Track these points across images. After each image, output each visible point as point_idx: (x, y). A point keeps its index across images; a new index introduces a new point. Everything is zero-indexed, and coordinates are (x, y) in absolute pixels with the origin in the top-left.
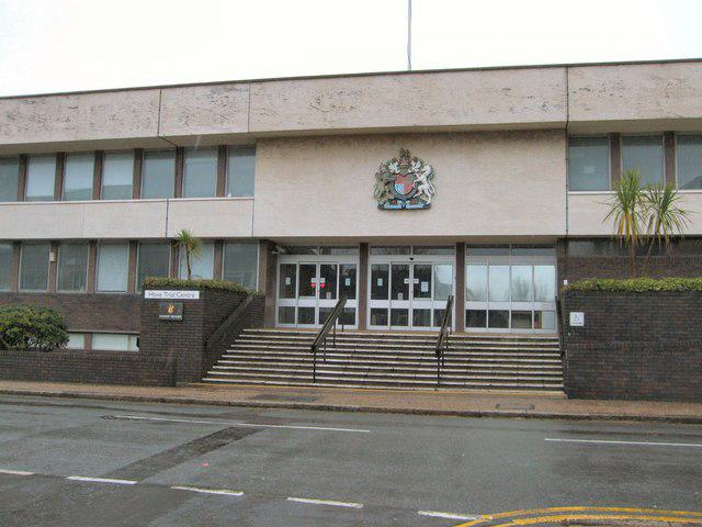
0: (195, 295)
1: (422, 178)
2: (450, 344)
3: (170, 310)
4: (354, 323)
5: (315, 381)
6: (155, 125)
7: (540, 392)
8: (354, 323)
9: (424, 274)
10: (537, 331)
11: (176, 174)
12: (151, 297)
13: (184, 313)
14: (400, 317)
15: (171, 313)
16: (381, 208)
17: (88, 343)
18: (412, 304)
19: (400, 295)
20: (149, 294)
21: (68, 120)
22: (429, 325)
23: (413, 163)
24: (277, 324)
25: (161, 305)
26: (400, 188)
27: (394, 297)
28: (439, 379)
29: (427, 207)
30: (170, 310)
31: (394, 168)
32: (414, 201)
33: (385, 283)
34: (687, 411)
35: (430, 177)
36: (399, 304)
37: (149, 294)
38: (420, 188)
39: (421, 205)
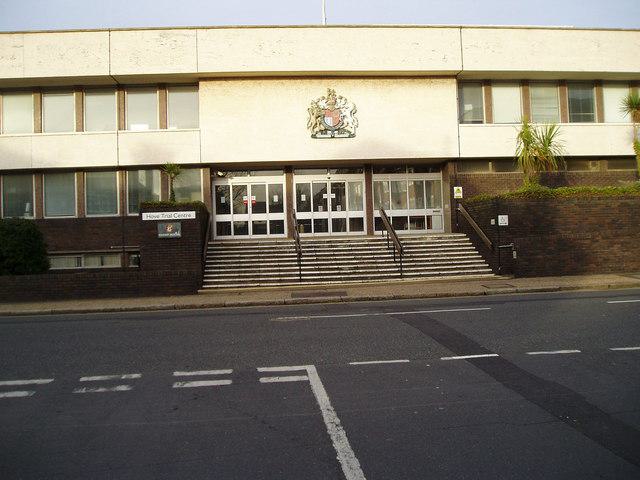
0: (192, 215)
1: (347, 113)
2: (386, 245)
3: (169, 229)
4: (363, 230)
5: (301, 280)
6: (107, 66)
7: (437, 278)
8: (363, 230)
9: (338, 189)
10: (430, 231)
11: (119, 109)
12: (149, 219)
13: (182, 232)
14: (321, 225)
15: (171, 232)
16: (314, 137)
17: (79, 264)
18: (330, 215)
19: (320, 208)
20: (146, 216)
21: (13, 58)
22: (345, 230)
23: (338, 101)
24: (216, 237)
25: (160, 226)
26: (329, 121)
27: (316, 210)
28: (300, 275)
29: (352, 136)
30: (169, 229)
31: (322, 104)
32: (339, 130)
33: (299, 198)
34: (440, 288)
35: (353, 112)
36: (320, 215)
37: (146, 216)
38: (345, 121)
39: (347, 135)
